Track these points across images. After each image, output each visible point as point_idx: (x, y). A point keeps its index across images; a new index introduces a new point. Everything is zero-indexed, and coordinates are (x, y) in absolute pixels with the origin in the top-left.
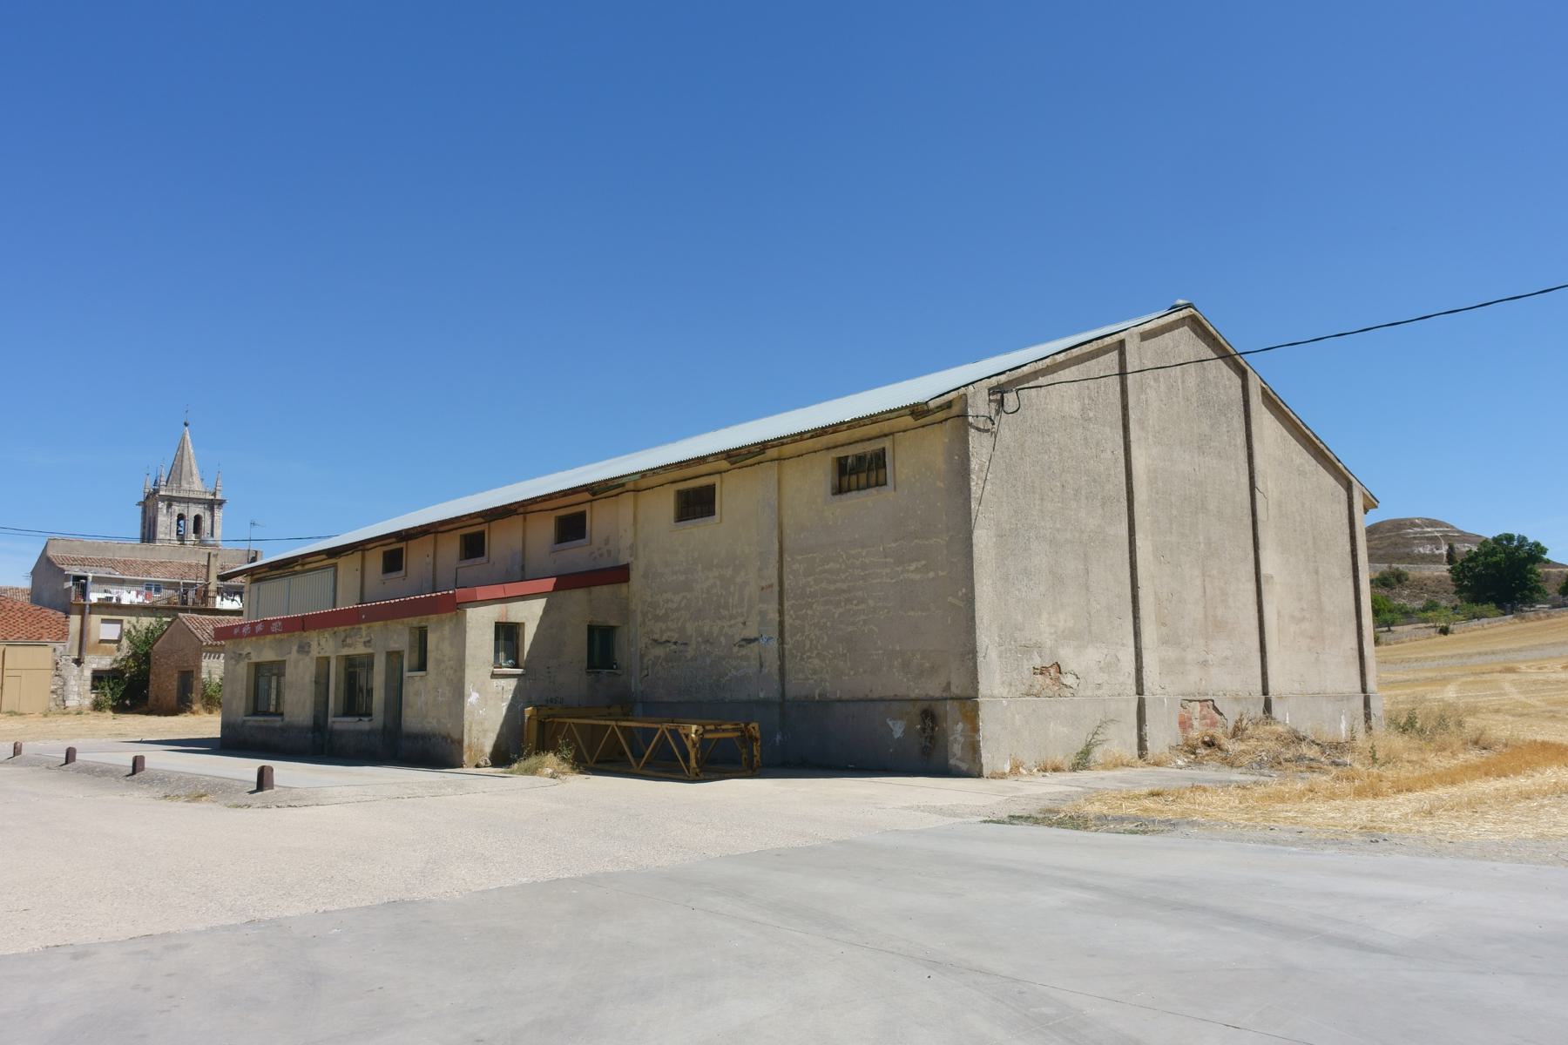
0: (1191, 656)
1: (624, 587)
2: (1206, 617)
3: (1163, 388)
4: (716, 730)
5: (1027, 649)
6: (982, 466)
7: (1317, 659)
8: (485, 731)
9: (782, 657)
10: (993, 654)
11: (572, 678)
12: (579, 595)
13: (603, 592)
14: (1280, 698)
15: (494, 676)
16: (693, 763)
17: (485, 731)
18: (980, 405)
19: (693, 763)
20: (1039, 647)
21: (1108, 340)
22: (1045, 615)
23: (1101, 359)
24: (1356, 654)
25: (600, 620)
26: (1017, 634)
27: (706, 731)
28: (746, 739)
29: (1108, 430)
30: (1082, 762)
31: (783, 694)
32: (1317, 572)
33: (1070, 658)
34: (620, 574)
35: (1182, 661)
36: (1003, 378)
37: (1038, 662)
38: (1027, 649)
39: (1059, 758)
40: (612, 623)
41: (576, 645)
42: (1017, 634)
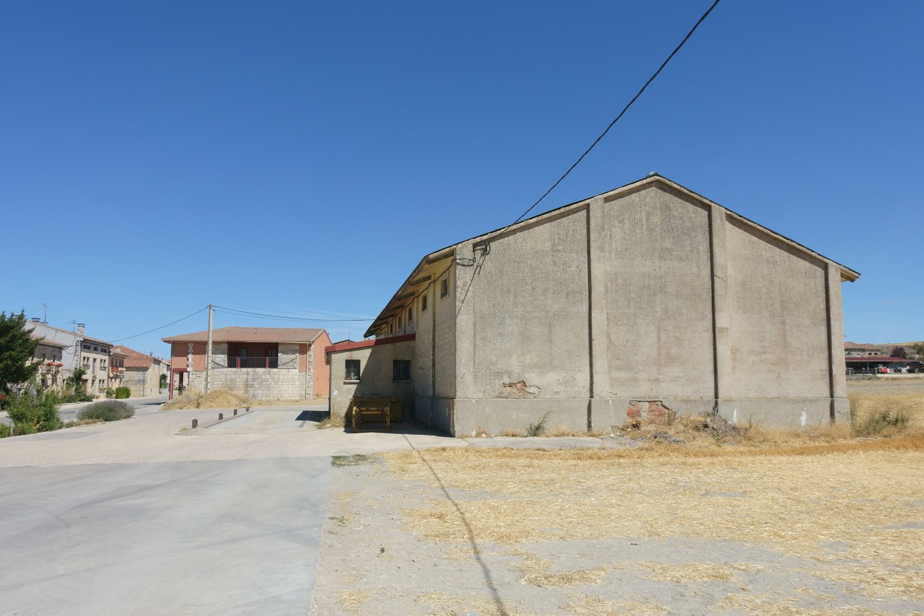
0: (641, 376)
1: (413, 342)
2: (659, 354)
3: (627, 225)
4: (367, 410)
5: (499, 374)
6: (465, 285)
7: (778, 377)
8: (341, 407)
9: (434, 376)
10: (469, 378)
11: (385, 384)
12: (389, 346)
13: (403, 345)
14: (729, 400)
15: (345, 383)
16: (354, 425)
17: (341, 407)
18: (465, 252)
19: (354, 425)
20: (509, 374)
21: (580, 204)
22: (514, 357)
23: (571, 217)
24: (827, 373)
25: (399, 358)
26: (492, 367)
27: (361, 411)
28: (383, 415)
29: (574, 255)
30: (536, 431)
31: (434, 394)
32: (783, 323)
33: (532, 378)
34: (412, 337)
35: (635, 380)
36: (485, 237)
37: (507, 380)
38: (499, 374)
39: (517, 430)
40: (407, 359)
41: (388, 368)
42: (492, 367)
